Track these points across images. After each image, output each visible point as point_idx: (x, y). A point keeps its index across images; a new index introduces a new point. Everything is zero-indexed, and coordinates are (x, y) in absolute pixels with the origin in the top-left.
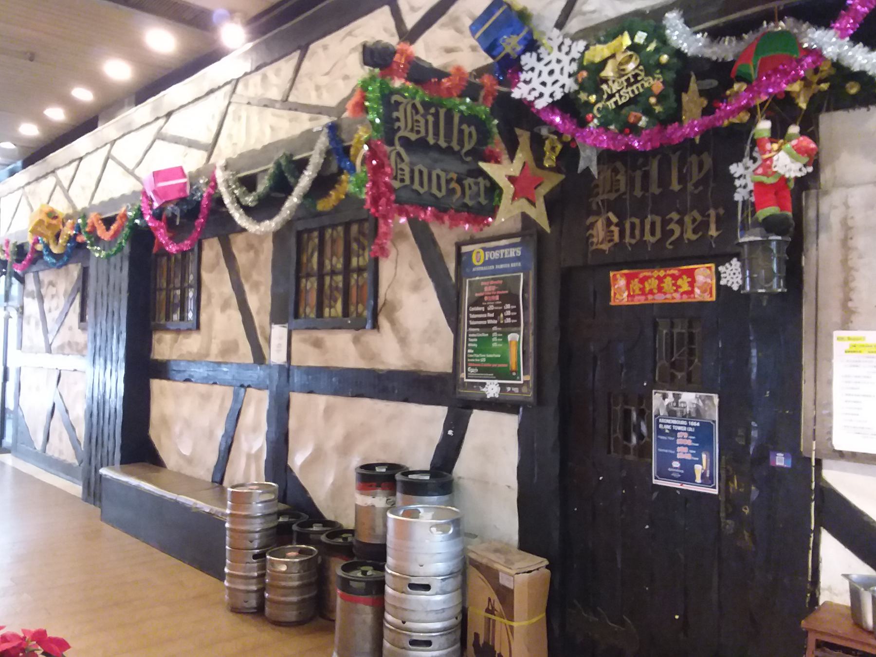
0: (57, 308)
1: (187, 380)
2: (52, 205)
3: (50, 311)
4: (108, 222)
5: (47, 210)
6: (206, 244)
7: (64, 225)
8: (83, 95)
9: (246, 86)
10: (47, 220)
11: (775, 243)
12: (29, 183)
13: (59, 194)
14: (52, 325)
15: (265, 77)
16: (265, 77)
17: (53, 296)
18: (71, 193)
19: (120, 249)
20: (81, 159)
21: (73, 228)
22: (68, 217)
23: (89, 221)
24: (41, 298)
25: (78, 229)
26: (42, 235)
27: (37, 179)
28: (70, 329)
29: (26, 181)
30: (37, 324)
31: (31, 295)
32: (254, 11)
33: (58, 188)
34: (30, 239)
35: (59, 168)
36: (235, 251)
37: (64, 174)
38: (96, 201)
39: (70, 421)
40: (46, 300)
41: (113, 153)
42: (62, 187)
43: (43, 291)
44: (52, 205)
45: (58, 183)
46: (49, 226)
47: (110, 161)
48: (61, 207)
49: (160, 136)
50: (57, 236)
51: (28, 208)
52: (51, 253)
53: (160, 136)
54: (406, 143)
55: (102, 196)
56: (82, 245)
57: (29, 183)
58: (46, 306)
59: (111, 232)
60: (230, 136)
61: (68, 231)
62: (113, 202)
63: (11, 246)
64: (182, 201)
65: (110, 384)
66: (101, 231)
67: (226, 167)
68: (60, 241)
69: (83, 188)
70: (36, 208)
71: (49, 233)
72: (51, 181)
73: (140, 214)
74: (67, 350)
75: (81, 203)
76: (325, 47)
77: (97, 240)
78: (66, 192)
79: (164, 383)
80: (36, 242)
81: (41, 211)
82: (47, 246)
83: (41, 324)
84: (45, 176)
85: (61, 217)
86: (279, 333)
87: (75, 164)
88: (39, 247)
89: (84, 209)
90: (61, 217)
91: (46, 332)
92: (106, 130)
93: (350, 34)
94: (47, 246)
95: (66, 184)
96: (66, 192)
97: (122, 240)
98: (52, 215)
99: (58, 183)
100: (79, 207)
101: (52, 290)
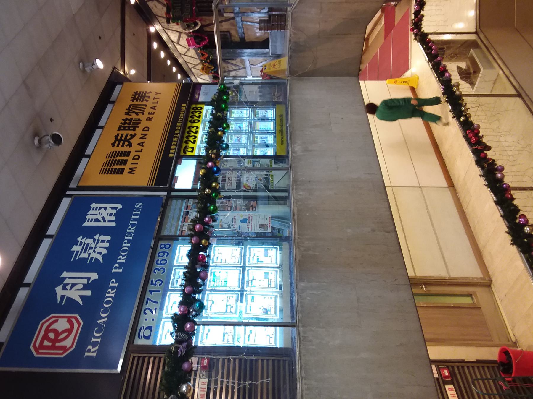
0: (232, 66)
1: (244, 33)
2: (200, 69)
3: (233, 68)
4: (203, 55)
5: (201, 71)
6: (205, 30)
7: (205, 66)
8: (169, 62)
9: (164, 26)
10: (204, 70)
11: (238, 360)
12: (194, 76)
13: (197, 67)
14: (237, 68)
15: (162, 22)
16: (162, 22)
17: (228, 67)
18: (196, 64)
19: (210, 51)
20: (186, 62)
21: (206, 63)
22: (203, 64)
23: (203, 59)
24: (229, 71)
25: (205, 62)
26: (209, 72)
27: (193, 73)
28: (237, 62)
29: (194, 76)
30: (238, 72)
31: (229, 74)
32: (145, 24)
33: (195, 67)
34: (211, 75)
35: (189, 68)
36: (206, 24)
37: (190, 66)
38: (197, 58)
39: (385, 39)
40: (230, 69)
41: (183, 54)
42: (194, 66)
43: (227, 70)
44: (200, 69)
45: (193, 67)
46: (206, 69)
47: (186, 54)
48: (200, 67)
49: (178, 43)
50: (209, 67)
51: (202, 76)
52: (214, 69)
53: (178, 43)
54: (182, 13)
55: (196, 56)
56: (210, 61)
57: (194, 76)
58: (232, 69)
59: (205, 54)
60: (177, 29)
61: (207, 64)
62: (197, 53)
63: (214, 80)
64: (195, 39)
65: (248, 53)
66: (206, 56)
67: (185, 30)
68: (210, 66)
69: (194, 61)
70: (202, 73)
71: (208, 69)
72: (193, 70)
73: (200, 48)
74: (244, 63)
75: (199, 61)
76: (155, 12)
77: (208, 58)
78: (196, 65)
79: (246, 38)
80: (211, 73)
81: (202, 72)
82: (212, 70)
83: (238, 71)
84: (192, 71)
85: (203, 66)
86: (225, 15)
87: (187, 63)
88: (213, 72)
89: (200, 61)
90: (203, 66)
91: (239, 69)
92: (176, 55)
93: (153, 8)
94: (212, 70)
95: (193, 65)
96: (196, 65)
97: (207, 52)
98: (203, 69)
99: (193, 67)
100: (199, 62)
101: (226, 68)
